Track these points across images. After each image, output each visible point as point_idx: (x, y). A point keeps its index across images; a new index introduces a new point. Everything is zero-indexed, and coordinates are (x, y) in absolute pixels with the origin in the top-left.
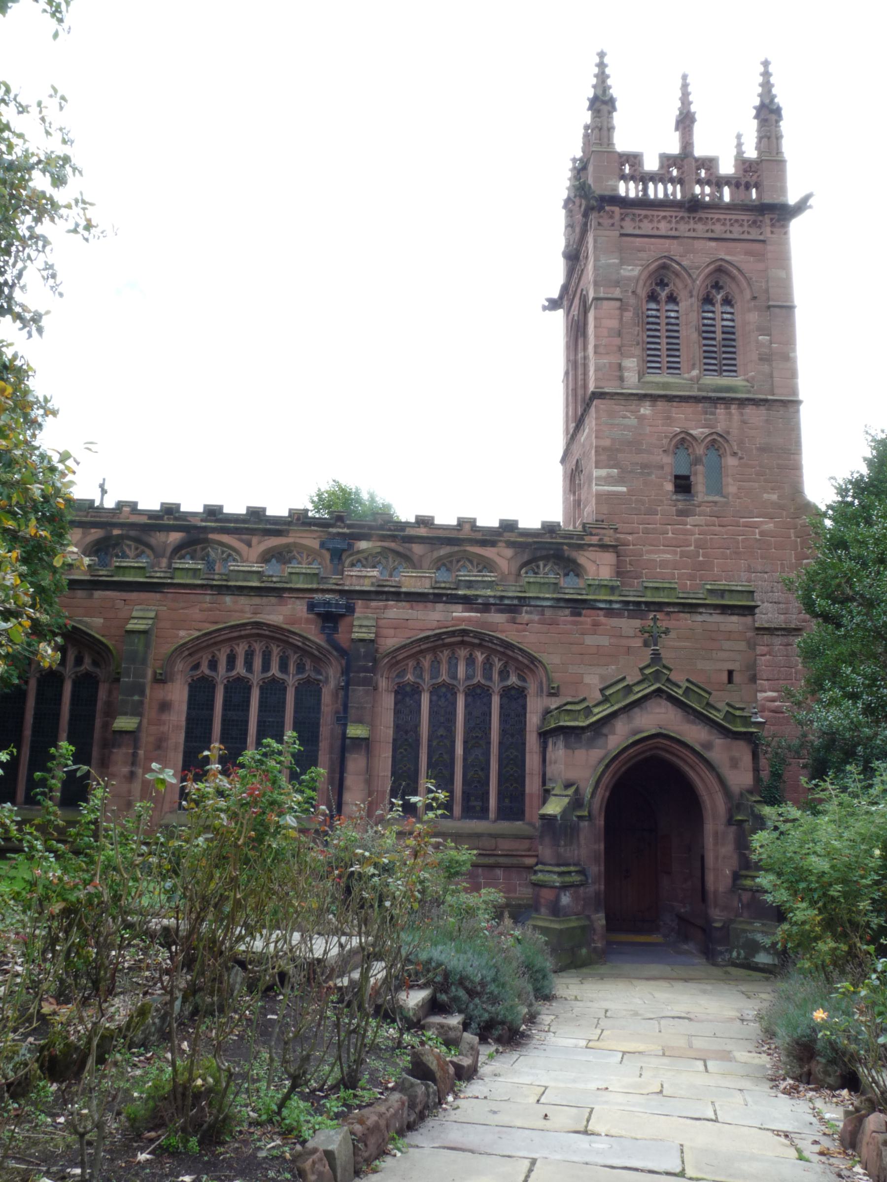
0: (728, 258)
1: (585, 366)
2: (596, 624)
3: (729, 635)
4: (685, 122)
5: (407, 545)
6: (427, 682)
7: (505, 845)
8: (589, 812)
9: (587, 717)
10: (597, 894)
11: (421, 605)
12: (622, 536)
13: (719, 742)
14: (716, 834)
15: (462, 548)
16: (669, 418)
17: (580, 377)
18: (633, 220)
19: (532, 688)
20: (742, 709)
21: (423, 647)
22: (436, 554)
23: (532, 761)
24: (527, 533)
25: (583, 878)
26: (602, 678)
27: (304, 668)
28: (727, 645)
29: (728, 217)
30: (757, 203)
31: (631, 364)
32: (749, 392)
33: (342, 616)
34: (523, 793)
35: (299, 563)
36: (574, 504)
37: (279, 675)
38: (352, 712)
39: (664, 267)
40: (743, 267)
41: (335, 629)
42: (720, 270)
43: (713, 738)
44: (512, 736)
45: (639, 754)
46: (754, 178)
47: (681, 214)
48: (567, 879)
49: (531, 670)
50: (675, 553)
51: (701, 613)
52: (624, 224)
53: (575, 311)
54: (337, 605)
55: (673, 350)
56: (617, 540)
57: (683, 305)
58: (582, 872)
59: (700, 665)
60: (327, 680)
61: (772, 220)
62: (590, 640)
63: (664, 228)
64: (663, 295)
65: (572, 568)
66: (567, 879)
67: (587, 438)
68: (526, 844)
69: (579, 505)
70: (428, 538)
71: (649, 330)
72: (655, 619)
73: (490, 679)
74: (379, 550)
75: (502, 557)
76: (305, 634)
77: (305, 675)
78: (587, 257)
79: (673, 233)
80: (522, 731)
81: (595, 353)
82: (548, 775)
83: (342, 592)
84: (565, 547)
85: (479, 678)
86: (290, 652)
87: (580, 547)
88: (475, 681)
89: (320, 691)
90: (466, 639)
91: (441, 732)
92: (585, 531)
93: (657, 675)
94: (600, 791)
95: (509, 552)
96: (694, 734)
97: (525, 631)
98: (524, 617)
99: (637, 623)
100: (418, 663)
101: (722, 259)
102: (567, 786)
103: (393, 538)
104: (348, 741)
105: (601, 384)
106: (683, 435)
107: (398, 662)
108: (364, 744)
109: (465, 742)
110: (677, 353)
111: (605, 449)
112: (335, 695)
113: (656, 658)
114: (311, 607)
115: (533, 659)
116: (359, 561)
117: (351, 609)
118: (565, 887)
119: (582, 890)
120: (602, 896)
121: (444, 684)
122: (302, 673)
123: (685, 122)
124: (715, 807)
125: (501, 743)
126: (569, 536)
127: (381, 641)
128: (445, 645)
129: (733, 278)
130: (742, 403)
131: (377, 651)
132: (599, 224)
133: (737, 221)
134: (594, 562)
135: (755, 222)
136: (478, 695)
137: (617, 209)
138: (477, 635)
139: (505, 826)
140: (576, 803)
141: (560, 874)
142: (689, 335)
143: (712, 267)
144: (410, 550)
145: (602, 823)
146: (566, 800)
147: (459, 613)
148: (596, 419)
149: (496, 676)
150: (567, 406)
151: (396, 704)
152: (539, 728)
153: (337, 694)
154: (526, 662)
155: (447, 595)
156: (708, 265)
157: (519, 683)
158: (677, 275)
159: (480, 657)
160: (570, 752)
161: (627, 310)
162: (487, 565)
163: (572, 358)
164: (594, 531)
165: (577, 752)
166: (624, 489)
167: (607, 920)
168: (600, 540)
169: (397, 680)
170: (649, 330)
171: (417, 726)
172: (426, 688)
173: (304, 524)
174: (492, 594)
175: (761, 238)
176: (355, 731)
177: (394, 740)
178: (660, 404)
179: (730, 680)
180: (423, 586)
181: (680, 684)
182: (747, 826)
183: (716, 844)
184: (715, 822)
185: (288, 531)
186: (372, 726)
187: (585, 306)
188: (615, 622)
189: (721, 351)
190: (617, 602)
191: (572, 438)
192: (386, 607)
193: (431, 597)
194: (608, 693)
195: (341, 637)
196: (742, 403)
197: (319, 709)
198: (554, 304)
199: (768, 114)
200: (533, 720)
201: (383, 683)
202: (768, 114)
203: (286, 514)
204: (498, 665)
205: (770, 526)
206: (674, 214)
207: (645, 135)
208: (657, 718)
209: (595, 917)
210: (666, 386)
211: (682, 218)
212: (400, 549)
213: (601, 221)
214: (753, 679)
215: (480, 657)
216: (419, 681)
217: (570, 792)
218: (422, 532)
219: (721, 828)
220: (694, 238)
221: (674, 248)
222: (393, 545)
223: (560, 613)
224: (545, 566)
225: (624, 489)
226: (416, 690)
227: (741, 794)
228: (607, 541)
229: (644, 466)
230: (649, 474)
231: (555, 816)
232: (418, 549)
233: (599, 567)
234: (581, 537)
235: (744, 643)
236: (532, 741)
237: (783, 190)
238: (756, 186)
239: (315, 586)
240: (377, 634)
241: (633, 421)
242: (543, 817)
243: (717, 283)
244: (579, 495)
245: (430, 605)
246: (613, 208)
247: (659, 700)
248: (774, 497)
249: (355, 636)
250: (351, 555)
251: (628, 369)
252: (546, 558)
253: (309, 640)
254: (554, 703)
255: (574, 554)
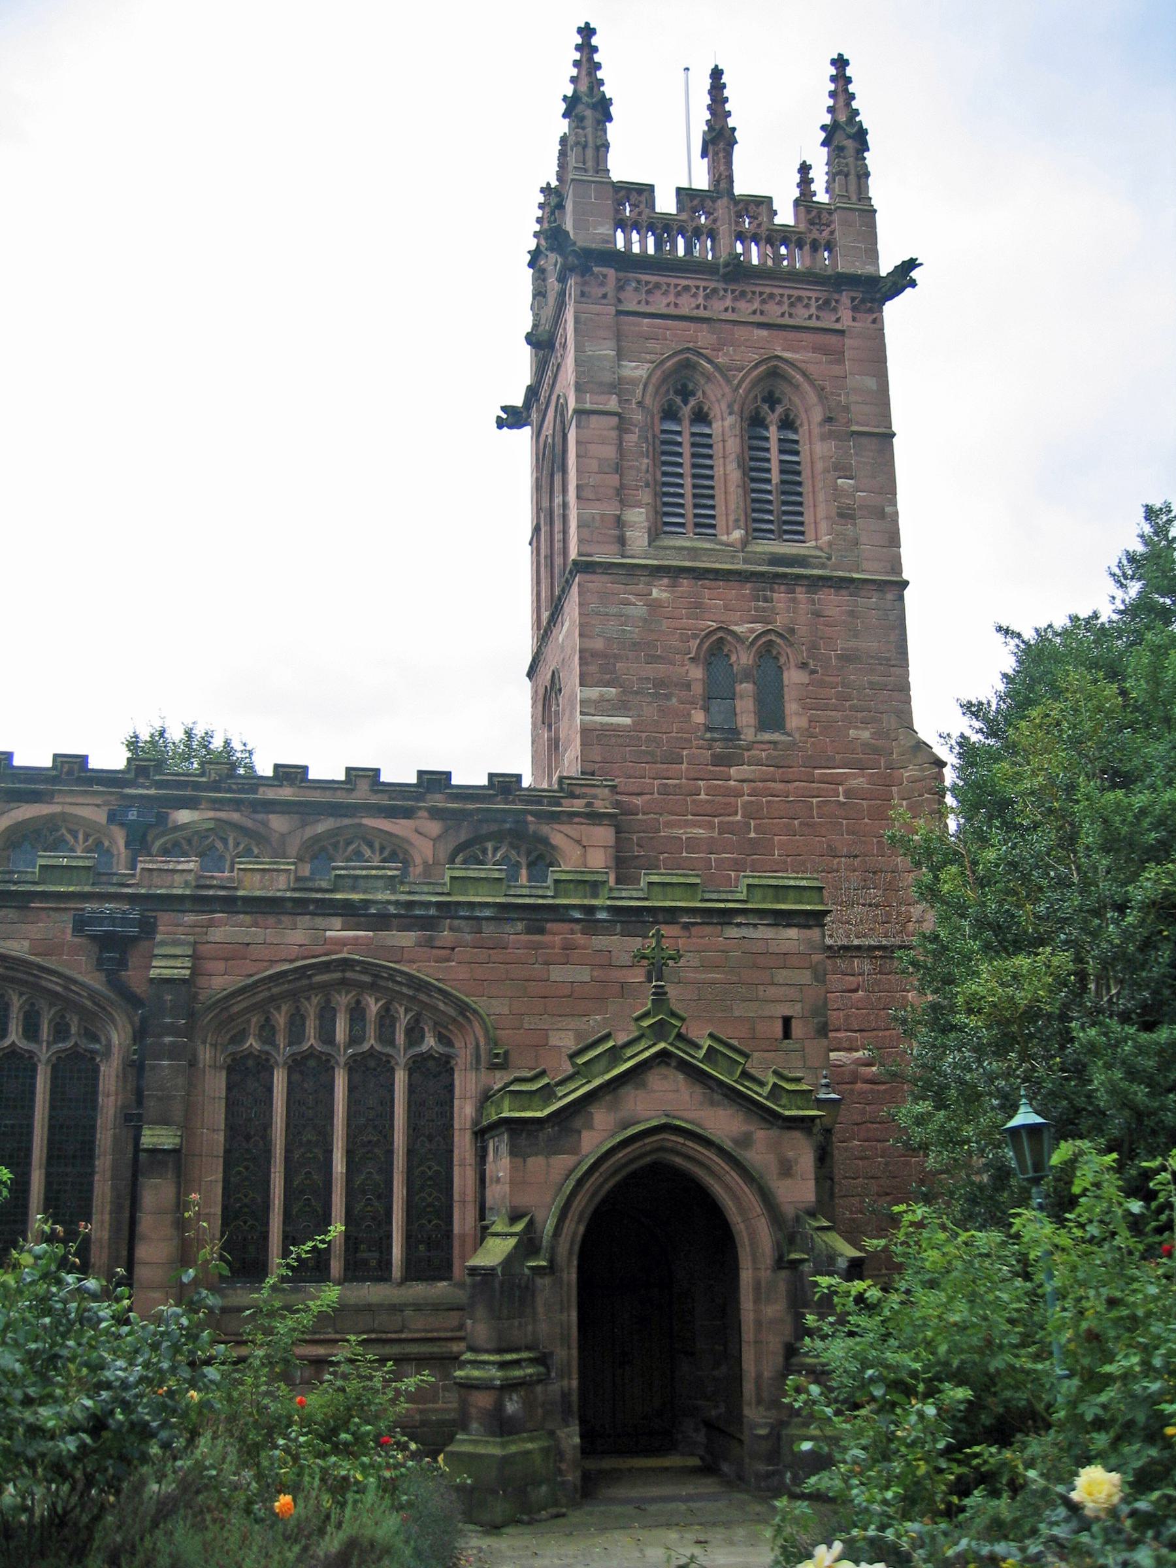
0: (787, 355)
1: (565, 518)
2: (568, 947)
3: (784, 960)
4: (719, 140)
5: (260, 817)
6: (283, 1051)
7: (418, 1324)
8: (552, 1261)
9: (547, 1104)
10: (565, 1395)
11: (271, 920)
12: (625, 798)
13: (761, 1135)
14: (757, 1287)
15: (357, 821)
16: (698, 605)
17: (558, 536)
18: (636, 289)
19: (463, 1055)
20: (798, 1080)
21: (275, 990)
22: (309, 832)
23: (463, 1179)
24: (468, 793)
25: (542, 1369)
26: (579, 1035)
27: (68, 1031)
28: (782, 975)
29: (787, 292)
30: (830, 272)
31: (638, 517)
32: (823, 566)
33: (134, 940)
34: (449, 1234)
35: (72, 850)
36: (547, 747)
37: (23, 1044)
38: (151, 1106)
39: (687, 365)
40: (811, 369)
41: (123, 964)
42: (774, 374)
43: (752, 1129)
44: (430, 1138)
45: (631, 1161)
46: (825, 234)
47: (713, 285)
48: (517, 1373)
49: (461, 1027)
50: (711, 826)
51: (739, 925)
52: (622, 295)
53: (548, 429)
54: (125, 921)
55: (704, 496)
56: (617, 804)
57: (717, 428)
58: (542, 1360)
59: (740, 1010)
60: (107, 1053)
61: (853, 299)
62: (558, 973)
63: (686, 305)
64: (686, 411)
65: (541, 857)
66: (517, 1373)
67: (566, 636)
68: (453, 1319)
69: (557, 747)
70: (295, 803)
71: (665, 463)
72: (659, 937)
73: (392, 1043)
74: (211, 825)
75: (422, 837)
76: (68, 972)
77: (69, 1044)
78: (564, 346)
79: (702, 313)
80: (447, 1129)
81: (578, 497)
82: (489, 1202)
83: (133, 899)
84: (530, 818)
85: (371, 1042)
86: (42, 1004)
87: (554, 817)
88: (365, 1047)
89: (96, 1070)
90: (349, 975)
91: (309, 1135)
92: (561, 790)
93: (659, 1030)
94: (569, 1226)
95: (434, 827)
96: (722, 1123)
97: (448, 960)
98: (446, 936)
99: (636, 943)
100: (267, 1019)
101: (777, 357)
102: (514, 1219)
103: (237, 805)
104: (143, 1156)
105: (587, 549)
106: (720, 634)
107: (231, 1018)
108: (175, 1161)
109: (349, 1153)
110: (710, 502)
111: (595, 654)
112: (123, 1077)
113: (660, 996)
114: (80, 925)
115: (463, 1008)
116: (176, 844)
117: (148, 928)
118: (509, 1387)
119: (539, 1389)
120: (575, 1398)
121: (311, 1054)
122: (64, 1040)
123: (719, 140)
124: (755, 1240)
125: (410, 1152)
126: (534, 796)
127: (202, 981)
128: (312, 987)
129: (797, 387)
130: (816, 583)
131: (195, 997)
132: (583, 294)
133: (799, 299)
134: (579, 842)
135: (827, 302)
136: (370, 1072)
137: (611, 273)
138: (366, 967)
139: (419, 1290)
140: (528, 1244)
141: (503, 1365)
142: (727, 472)
143: (762, 368)
144: (265, 824)
145: (574, 1276)
146: (512, 1242)
147: (336, 931)
148: (581, 605)
149: (400, 1038)
150: (538, 582)
151: (229, 1089)
152: (476, 1122)
153: (125, 1076)
154: (452, 1012)
155: (317, 900)
156: (756, 366)
157: (441, 1049)
158: (709, 378)
159: (373, 1007)
160: (519, 1160)
161: (628, 431)
162: (396, 852)
163: (545, 504)
164: (578, 791)
165: (531, 1161)
166: (628, 721)
167: (582, 1437)
168: (589, 805)
169: (232, 1049)
170: (665, 463)
171: (267, 1126)
172: (280, 1060)
173: (80, 781)
174: (393, 898)
175: (838, 326)
176: (155, 1137)
177: (227, 1152)
178: (685, 583)
179: (787, 1035)
180: (279, 887)
181: (700, 1042)
182: (807, 1268)
183: (757, 1301)
184: (754, 1267)
185: (52, 794)
186: (187, 1128)
187: (563, 422)
188: (600, 942)
189: (776, 504)
190: (603, 908)
191: (544, 631)
192: (211, 924)
193: (289, 905)
194: (581, 1061)
195: (133, 977)
196: (816, 583)
197: (94, 1101)
198: (511, 418)
199: (846, 137)
200: (464, 1111)
201: (206, 1055)
202: (846, 137)
203: (48, 763)
204: (403, 1019)
205: (859, 782)
206: (702, 284)
207: (654, 152)
208: (666, 1099)
209: (561, 1433)
210: (694, 552)
211: (715, 291)
212: (248, 823)
213: (586, 289)
214: (823, 1030)
215: (373, 1007)
216: (267, 1048)
217: (519, 1227)
218: (286, 793)
219: (766, 1274)
220: (735, 322)
221: (704, 337)
222: (235, 816)
223: (508, 928)
224: (496, 850)
225: (628, 721)
226: (264, 1066)
227: (797, 1219)
228: (601, 807)
229: (659, 683)
230: (668, 697)
231: (493, 1269)
232: (278, 823)
233: (584, 851)
234: (556, 802)
235: (808, 973)
236: (463, 1145)
237: (873, 254)
238: (829, 247)
239: (87, 889)
240: (195, 971)
241: (638, 610)
242: (473, 1271)
243: (771, 393)
244: (557, 730)
245: (285, 919)
246: (605, 270)
247: (664, 1070)
248: (865, 735)
249: (153, 973)
250: (163, 834)
251: (632, 525)
252: (498, 837)
253: (75, 982)
254: (499, 1080)
255: (545, 829)
